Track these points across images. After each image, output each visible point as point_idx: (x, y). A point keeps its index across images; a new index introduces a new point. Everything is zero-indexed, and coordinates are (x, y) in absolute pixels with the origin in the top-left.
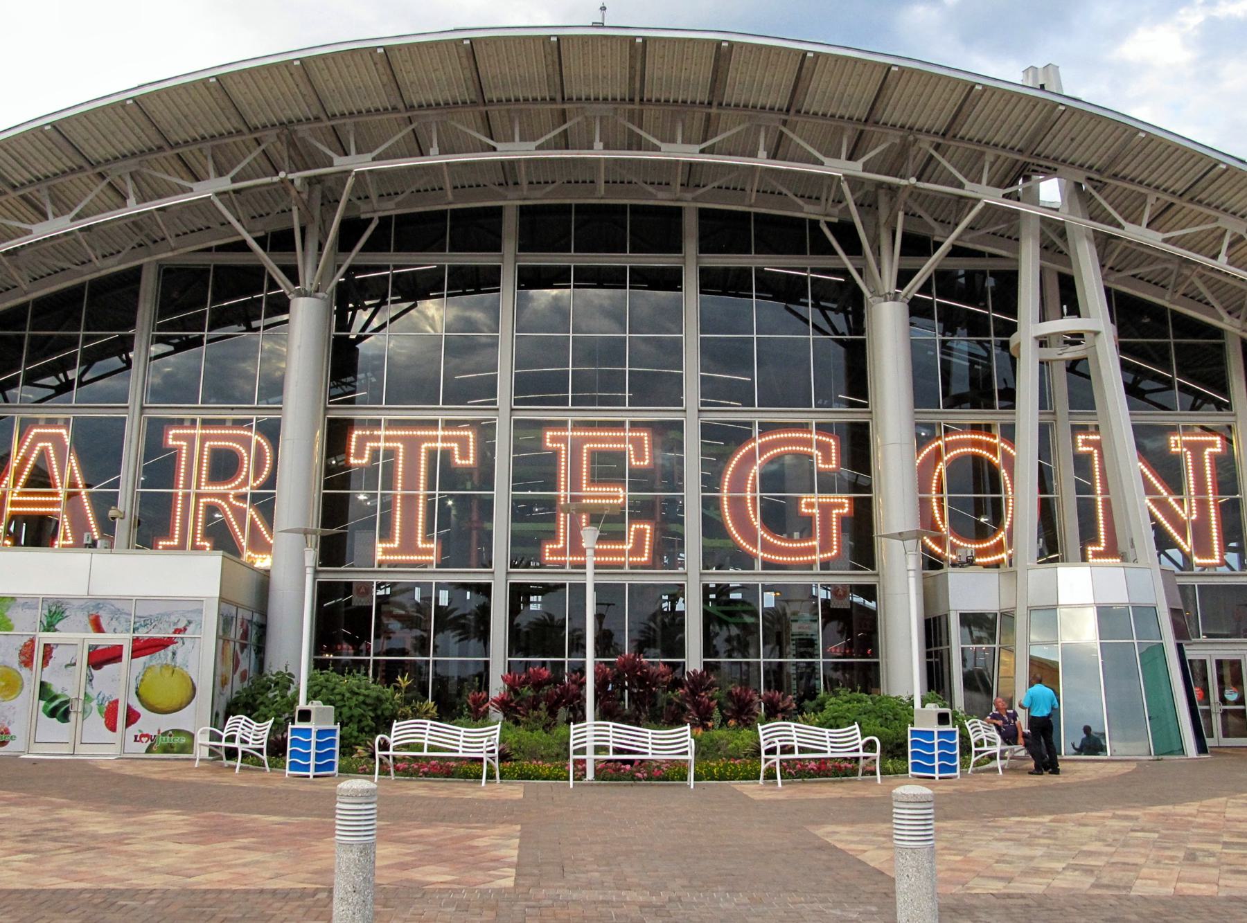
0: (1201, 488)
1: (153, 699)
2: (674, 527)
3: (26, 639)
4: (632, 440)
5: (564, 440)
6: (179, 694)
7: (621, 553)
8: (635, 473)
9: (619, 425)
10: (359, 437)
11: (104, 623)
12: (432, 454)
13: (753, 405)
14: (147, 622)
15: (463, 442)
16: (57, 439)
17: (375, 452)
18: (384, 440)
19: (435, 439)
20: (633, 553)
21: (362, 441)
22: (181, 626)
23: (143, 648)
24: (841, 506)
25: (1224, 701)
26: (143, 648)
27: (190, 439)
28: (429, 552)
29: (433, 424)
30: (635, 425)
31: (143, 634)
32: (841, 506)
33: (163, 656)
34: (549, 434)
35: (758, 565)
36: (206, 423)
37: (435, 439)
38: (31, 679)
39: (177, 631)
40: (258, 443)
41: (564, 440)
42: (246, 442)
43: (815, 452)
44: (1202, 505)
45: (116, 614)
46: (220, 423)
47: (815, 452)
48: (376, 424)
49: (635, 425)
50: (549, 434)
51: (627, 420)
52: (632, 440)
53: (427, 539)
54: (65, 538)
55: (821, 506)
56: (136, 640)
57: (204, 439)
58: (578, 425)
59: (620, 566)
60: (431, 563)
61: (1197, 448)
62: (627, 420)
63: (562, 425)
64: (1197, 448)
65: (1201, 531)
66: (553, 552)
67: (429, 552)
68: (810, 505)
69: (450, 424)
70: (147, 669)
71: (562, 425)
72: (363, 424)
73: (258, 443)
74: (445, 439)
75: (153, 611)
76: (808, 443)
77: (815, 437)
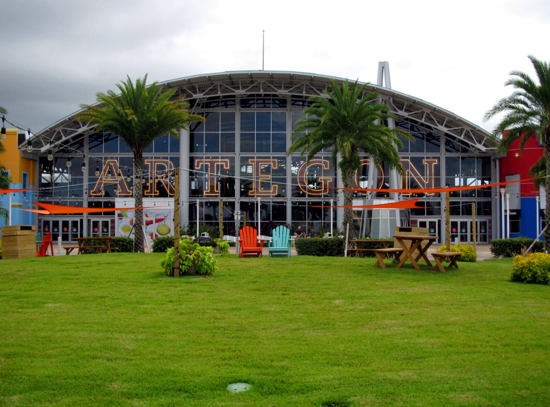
0: (430, 174)
1: (161, 232)
2: (386, 196)
3: (131, 219)
4: (273, 162)
5: (254, 162)
6: (167, 231)
7: (270, 193)
8: (273, 171)
9: (269, 158)
10: (197, 161)
11: (148, 215)
12: (218, 166)
13: (168, 152)
14: (158, 215)
15: (226, 162)
16: (114, 162)
17: (202, 165)
18: (204, 162)
19: (218, 162)
20: (273, 193)
21: (198, 162)
22: (166, 216)
23: (158, 221)
24: (330, 180)
25: (461, 232)
26: (158, 221)
27: (151, 162)
28: (218, 193)
29: (218, 158)
30: (273, 158)
31: (157, 217)
32: (330, 180)
33: (162, 222)
34: (250, 160)
35: (307, 196)
36: (155, 158)
37: (218, 162)
38: (457, 382)
39: (165, 217)
40: (170, 163)
41: (254, 162)
42: (167, 163)
43: (323, 164)
44: (430, 179)
45: (151, 213)
46: (159, 158)
47: (323, 164)
48: (202, 158)
49: (273, 158)
50: (250, 160)
51: (425, 156)
52: (273, 162)
53: (217, 189)
54: (119, 190)
55: (324, 180)
56: (156, 219)
57: (155, 162)
58: (258, 158)
59: (269, 196)
60: (219, 196)
61: (430, 163)
62: (425, 156)
63: (253, 158)
64: (430, 163)
65: (429, 185)
66: (251, 193)
67: (218, 193)
68: (321, 180)
69: (222, 158)
70: (159, 226)
71: (253, 158)
72: (197, 158)
73: (170, 163)
74: (221, 162)
75: (159, 212)
76: (321, 162)
77: (272, 160)
